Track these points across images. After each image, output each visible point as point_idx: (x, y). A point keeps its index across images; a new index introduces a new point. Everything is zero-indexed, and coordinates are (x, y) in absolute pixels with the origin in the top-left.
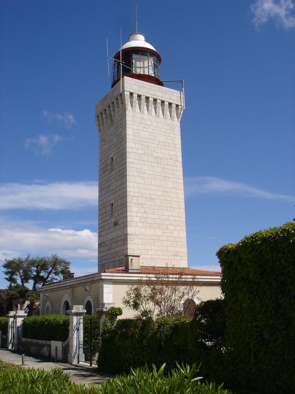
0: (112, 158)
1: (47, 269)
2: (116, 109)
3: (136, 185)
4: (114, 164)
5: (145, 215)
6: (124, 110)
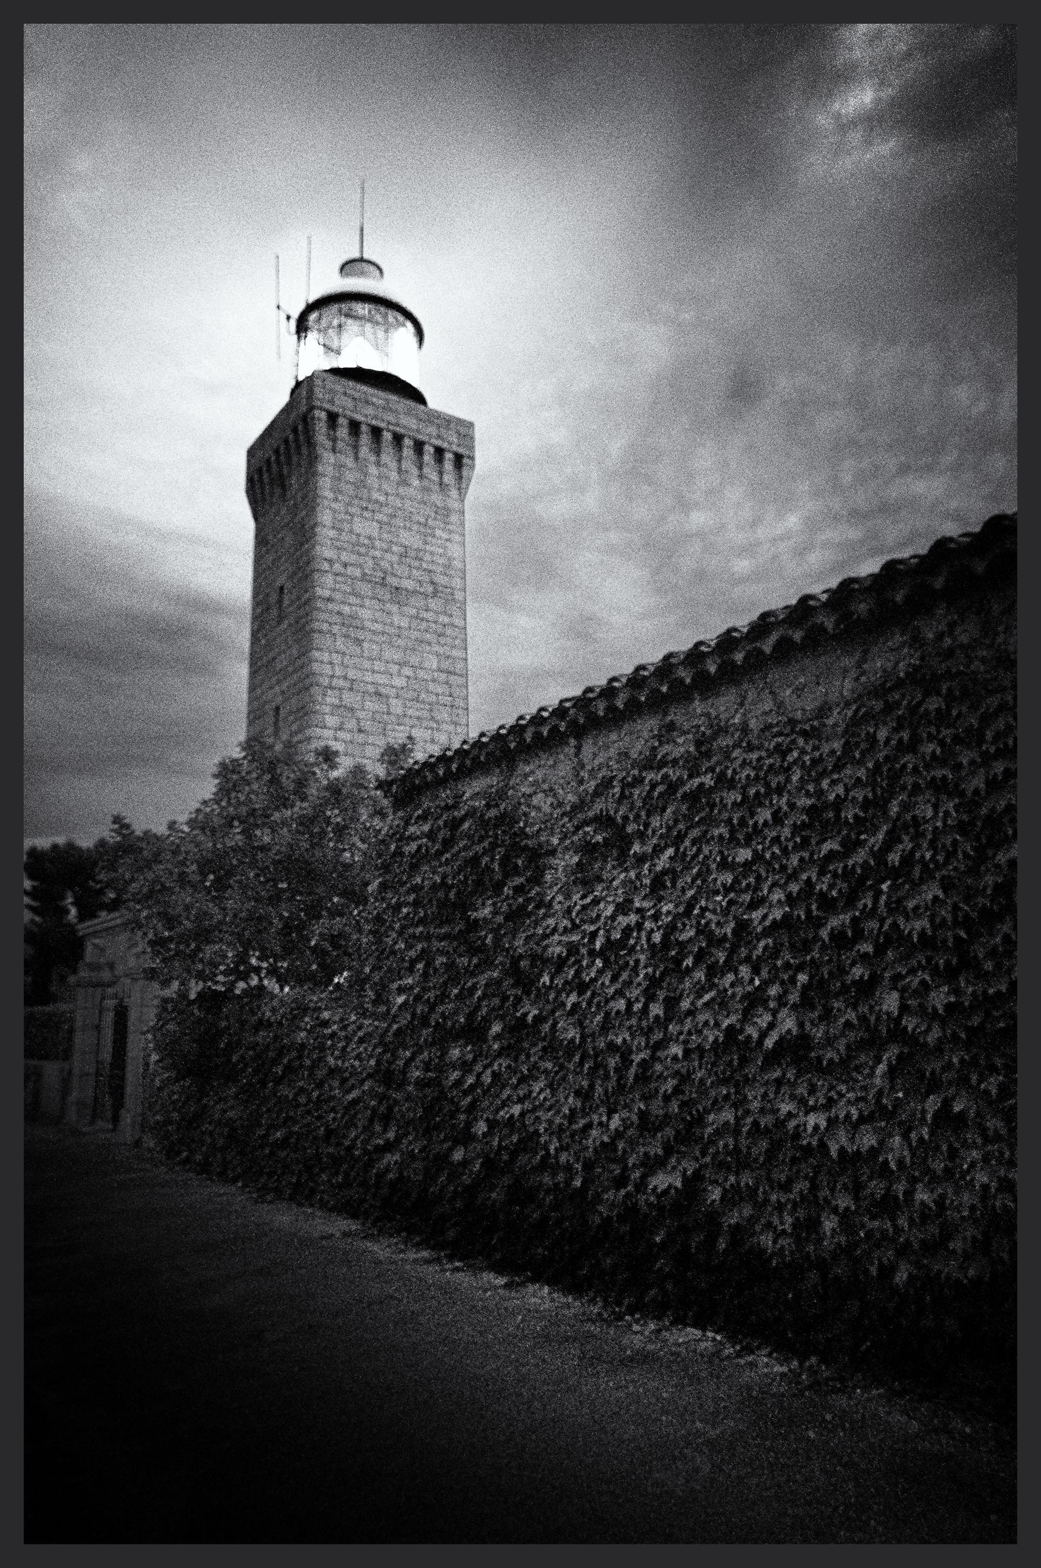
0: (282, 588)
1: (239, 1081)
2: (295, 459)
3: (336, 658)
4: (286, 602)
5: (360, 738)
6: (313, 459)
